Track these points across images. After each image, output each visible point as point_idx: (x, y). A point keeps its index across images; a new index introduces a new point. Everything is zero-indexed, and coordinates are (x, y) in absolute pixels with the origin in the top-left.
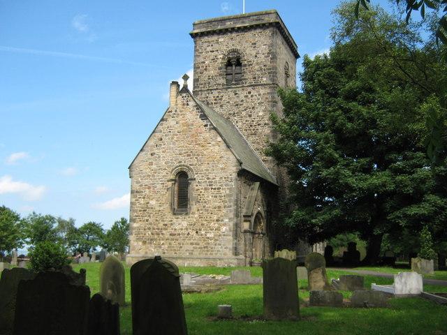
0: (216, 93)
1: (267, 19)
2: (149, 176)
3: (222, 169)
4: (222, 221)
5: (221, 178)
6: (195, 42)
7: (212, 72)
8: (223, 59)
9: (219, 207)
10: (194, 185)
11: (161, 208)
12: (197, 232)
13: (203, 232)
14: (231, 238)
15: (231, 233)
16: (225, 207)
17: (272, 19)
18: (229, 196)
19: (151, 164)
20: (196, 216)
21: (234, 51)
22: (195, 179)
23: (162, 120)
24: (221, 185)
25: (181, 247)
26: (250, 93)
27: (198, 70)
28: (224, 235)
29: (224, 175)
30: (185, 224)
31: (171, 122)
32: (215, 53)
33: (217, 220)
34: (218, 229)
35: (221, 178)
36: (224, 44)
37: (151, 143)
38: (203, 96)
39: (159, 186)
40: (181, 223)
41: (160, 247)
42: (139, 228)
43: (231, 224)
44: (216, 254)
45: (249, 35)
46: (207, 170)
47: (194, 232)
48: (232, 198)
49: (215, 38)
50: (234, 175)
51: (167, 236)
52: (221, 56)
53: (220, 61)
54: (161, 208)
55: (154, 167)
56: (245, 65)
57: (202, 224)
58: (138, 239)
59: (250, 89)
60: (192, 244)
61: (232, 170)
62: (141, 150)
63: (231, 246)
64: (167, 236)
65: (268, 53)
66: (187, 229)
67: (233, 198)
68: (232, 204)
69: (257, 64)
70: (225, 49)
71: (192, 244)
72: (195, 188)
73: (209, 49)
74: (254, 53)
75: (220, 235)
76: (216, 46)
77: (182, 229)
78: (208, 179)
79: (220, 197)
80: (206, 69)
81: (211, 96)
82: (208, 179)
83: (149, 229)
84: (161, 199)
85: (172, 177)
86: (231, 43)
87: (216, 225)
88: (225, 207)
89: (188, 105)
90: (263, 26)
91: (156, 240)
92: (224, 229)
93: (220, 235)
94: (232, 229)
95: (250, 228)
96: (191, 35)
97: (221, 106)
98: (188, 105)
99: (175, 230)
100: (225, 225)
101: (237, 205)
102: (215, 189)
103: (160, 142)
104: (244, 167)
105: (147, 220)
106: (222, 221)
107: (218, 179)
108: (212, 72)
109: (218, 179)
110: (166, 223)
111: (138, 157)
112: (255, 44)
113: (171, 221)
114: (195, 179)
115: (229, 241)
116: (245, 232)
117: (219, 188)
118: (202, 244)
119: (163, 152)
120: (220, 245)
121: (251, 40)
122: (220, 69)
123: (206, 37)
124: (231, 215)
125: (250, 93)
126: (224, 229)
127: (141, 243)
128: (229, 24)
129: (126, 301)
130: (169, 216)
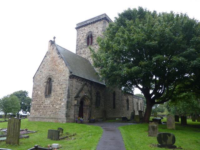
0: (83, 49)
1: (102, 17)
2: (39, 81)
3: (64, 75)
4: (62, 100)
5: (63, 80)
6: (77, 31)
7: (82, 41)
8: (86, 35)
9: (61, 93)
10: (53, 83)
11: (42, 95)
12: (53, 106)
13: (55, 106)
14: (65, 108)
15: (65, 106)
16: (63, 93)
17: (104, 17)
18: (66, 88)
19: (40, 76)
20: (53, 98)
21: (90, 32)
22: (54, 81)
23: (45, 57)
24: (63, 83)
25: (47, 113)
26: (95, 47)
27: (78, 41)
28: (62, 107)
29: (64, 78)
30: (49, 102)
31: (48, 57)
32: (84, 34)
33: (60, 100)
34: (60, 104)
35: (63, 80)
36: (87, 30)
37: (41, 67)
38: (79, 51)
39: (42, 85)
40: (48, 101)
41: (40, 113)
42: (34, 104)
43: (65, 101)
44: (59, 116)
45: (95, 24)
46: (58, 77)
47: (52, 106)
48: (67, 89)
49: (84, 28)
50: (68, 78)
51: (43, 108)
52: (86, 35)
53: (85, 36)
54: (42, 95)
55: (41, 77)
56: (94, 37)
57: (55, 102)
58: (33, 109)
59: (95, 46)
60: (50, 111)
61: (68, 75)
62: (38, 70)
63: (65, 112)
64: (43, 108)
65: (102, 30)
66: (49, 104)
67: (67, 89)
68: (66, 92)
69: (98, 35)
70: (87, 32)
71: (50, 111)
72: (54, 84)
73: (82, 33)
74: (97, 31)
75: (61, 107)
76: (84, 31)
77: (48, 104)
78: (58, 80)
79: (62, 88)
80: (80, 41)
81: (82, 50)
82: (58, 80)
83: (37, 104)
84: (41, 92)
85: (46, 81)
86: (89, 29)
87: (60, 102)
88: (63, 93)
89: (54, 49)
90: (100, 20)
91: (39, 109)
92: (62, 104)
93: (61, 107)
94: (65, 104)
95: (77, 103)
96: (75, 28)
97: (85, 54)
98: (54, 49)
99: (45, 104)
100: (63, 102)
101: (68, 92)
102: (60, 85)
103: (44, 66)
104: (73, 74)
105: (37, 100)
106: (62, 100)
107: (62, 80)
108: (82, 41)
109: (62, 80)
110: (42, 101)
111: (37, 74)
112: (97, 28)
113: (44, 100)
114: (54, 81)
115: (64, 110)
116: (75, 105)
117: (62, 85)
118: (54, 112)
119: (45, 70)
120: (60, 112)
121: (96, 26)
122: (85, 39)
123: (81, 29)
124: (66, 97)
125: (95, 47)
126: (62, 104)
127: (34, 111)
128: (88, 22)
129: (150, 119)
130: (44, 98)
